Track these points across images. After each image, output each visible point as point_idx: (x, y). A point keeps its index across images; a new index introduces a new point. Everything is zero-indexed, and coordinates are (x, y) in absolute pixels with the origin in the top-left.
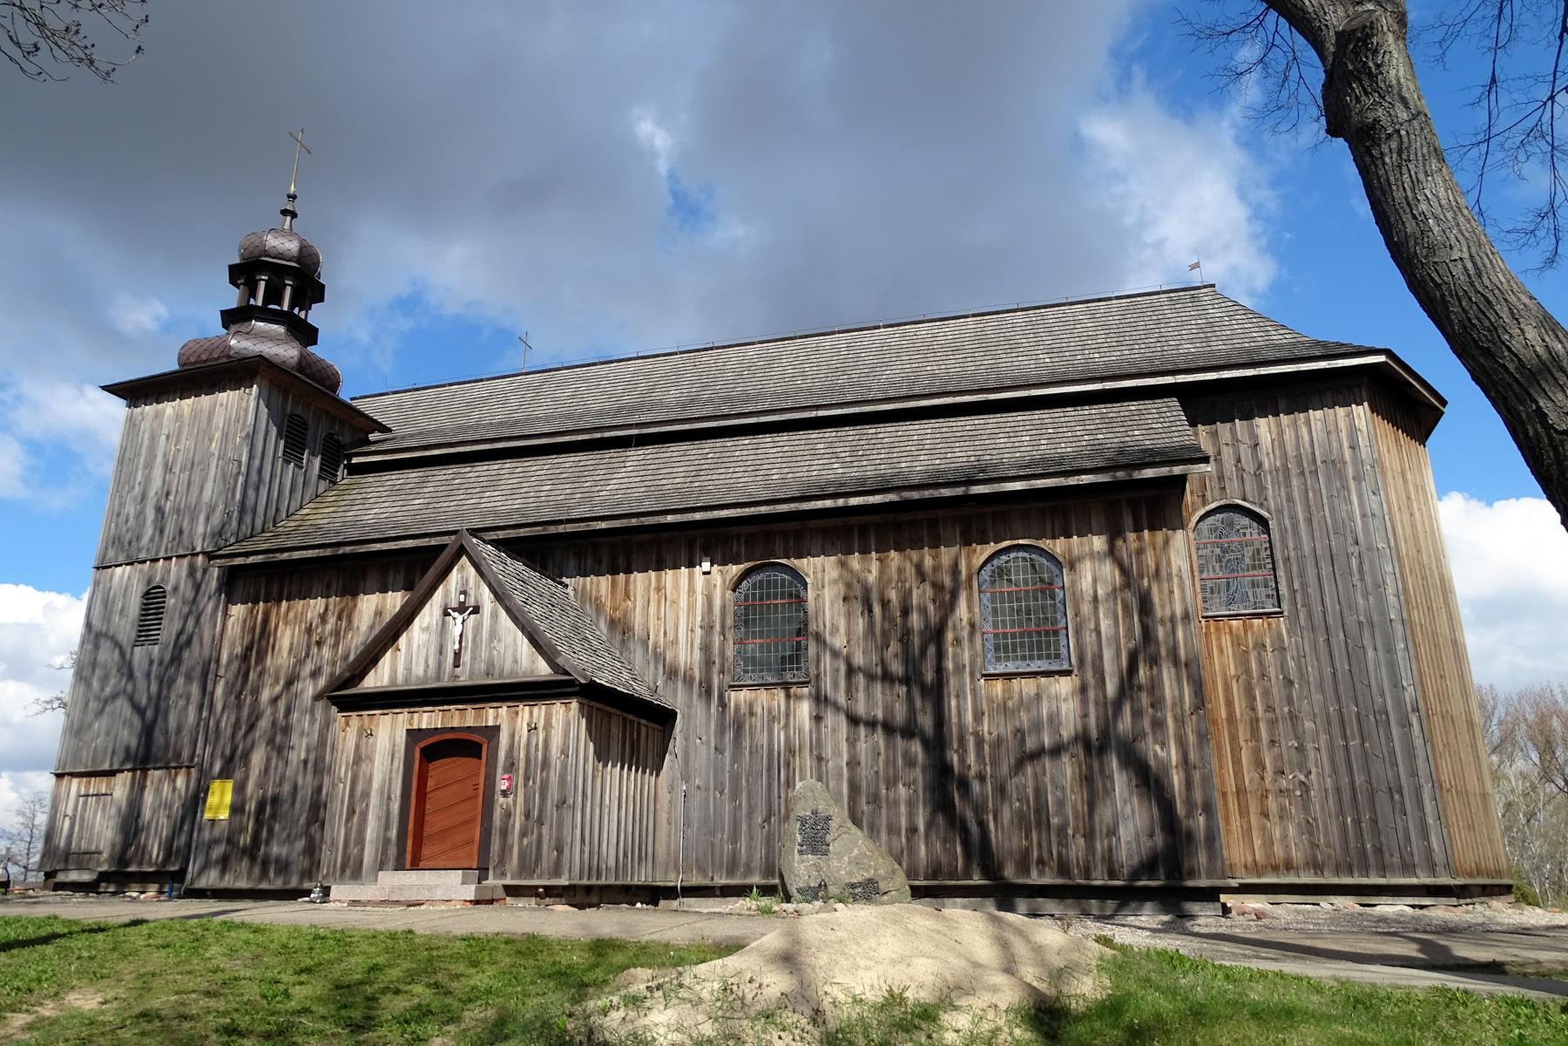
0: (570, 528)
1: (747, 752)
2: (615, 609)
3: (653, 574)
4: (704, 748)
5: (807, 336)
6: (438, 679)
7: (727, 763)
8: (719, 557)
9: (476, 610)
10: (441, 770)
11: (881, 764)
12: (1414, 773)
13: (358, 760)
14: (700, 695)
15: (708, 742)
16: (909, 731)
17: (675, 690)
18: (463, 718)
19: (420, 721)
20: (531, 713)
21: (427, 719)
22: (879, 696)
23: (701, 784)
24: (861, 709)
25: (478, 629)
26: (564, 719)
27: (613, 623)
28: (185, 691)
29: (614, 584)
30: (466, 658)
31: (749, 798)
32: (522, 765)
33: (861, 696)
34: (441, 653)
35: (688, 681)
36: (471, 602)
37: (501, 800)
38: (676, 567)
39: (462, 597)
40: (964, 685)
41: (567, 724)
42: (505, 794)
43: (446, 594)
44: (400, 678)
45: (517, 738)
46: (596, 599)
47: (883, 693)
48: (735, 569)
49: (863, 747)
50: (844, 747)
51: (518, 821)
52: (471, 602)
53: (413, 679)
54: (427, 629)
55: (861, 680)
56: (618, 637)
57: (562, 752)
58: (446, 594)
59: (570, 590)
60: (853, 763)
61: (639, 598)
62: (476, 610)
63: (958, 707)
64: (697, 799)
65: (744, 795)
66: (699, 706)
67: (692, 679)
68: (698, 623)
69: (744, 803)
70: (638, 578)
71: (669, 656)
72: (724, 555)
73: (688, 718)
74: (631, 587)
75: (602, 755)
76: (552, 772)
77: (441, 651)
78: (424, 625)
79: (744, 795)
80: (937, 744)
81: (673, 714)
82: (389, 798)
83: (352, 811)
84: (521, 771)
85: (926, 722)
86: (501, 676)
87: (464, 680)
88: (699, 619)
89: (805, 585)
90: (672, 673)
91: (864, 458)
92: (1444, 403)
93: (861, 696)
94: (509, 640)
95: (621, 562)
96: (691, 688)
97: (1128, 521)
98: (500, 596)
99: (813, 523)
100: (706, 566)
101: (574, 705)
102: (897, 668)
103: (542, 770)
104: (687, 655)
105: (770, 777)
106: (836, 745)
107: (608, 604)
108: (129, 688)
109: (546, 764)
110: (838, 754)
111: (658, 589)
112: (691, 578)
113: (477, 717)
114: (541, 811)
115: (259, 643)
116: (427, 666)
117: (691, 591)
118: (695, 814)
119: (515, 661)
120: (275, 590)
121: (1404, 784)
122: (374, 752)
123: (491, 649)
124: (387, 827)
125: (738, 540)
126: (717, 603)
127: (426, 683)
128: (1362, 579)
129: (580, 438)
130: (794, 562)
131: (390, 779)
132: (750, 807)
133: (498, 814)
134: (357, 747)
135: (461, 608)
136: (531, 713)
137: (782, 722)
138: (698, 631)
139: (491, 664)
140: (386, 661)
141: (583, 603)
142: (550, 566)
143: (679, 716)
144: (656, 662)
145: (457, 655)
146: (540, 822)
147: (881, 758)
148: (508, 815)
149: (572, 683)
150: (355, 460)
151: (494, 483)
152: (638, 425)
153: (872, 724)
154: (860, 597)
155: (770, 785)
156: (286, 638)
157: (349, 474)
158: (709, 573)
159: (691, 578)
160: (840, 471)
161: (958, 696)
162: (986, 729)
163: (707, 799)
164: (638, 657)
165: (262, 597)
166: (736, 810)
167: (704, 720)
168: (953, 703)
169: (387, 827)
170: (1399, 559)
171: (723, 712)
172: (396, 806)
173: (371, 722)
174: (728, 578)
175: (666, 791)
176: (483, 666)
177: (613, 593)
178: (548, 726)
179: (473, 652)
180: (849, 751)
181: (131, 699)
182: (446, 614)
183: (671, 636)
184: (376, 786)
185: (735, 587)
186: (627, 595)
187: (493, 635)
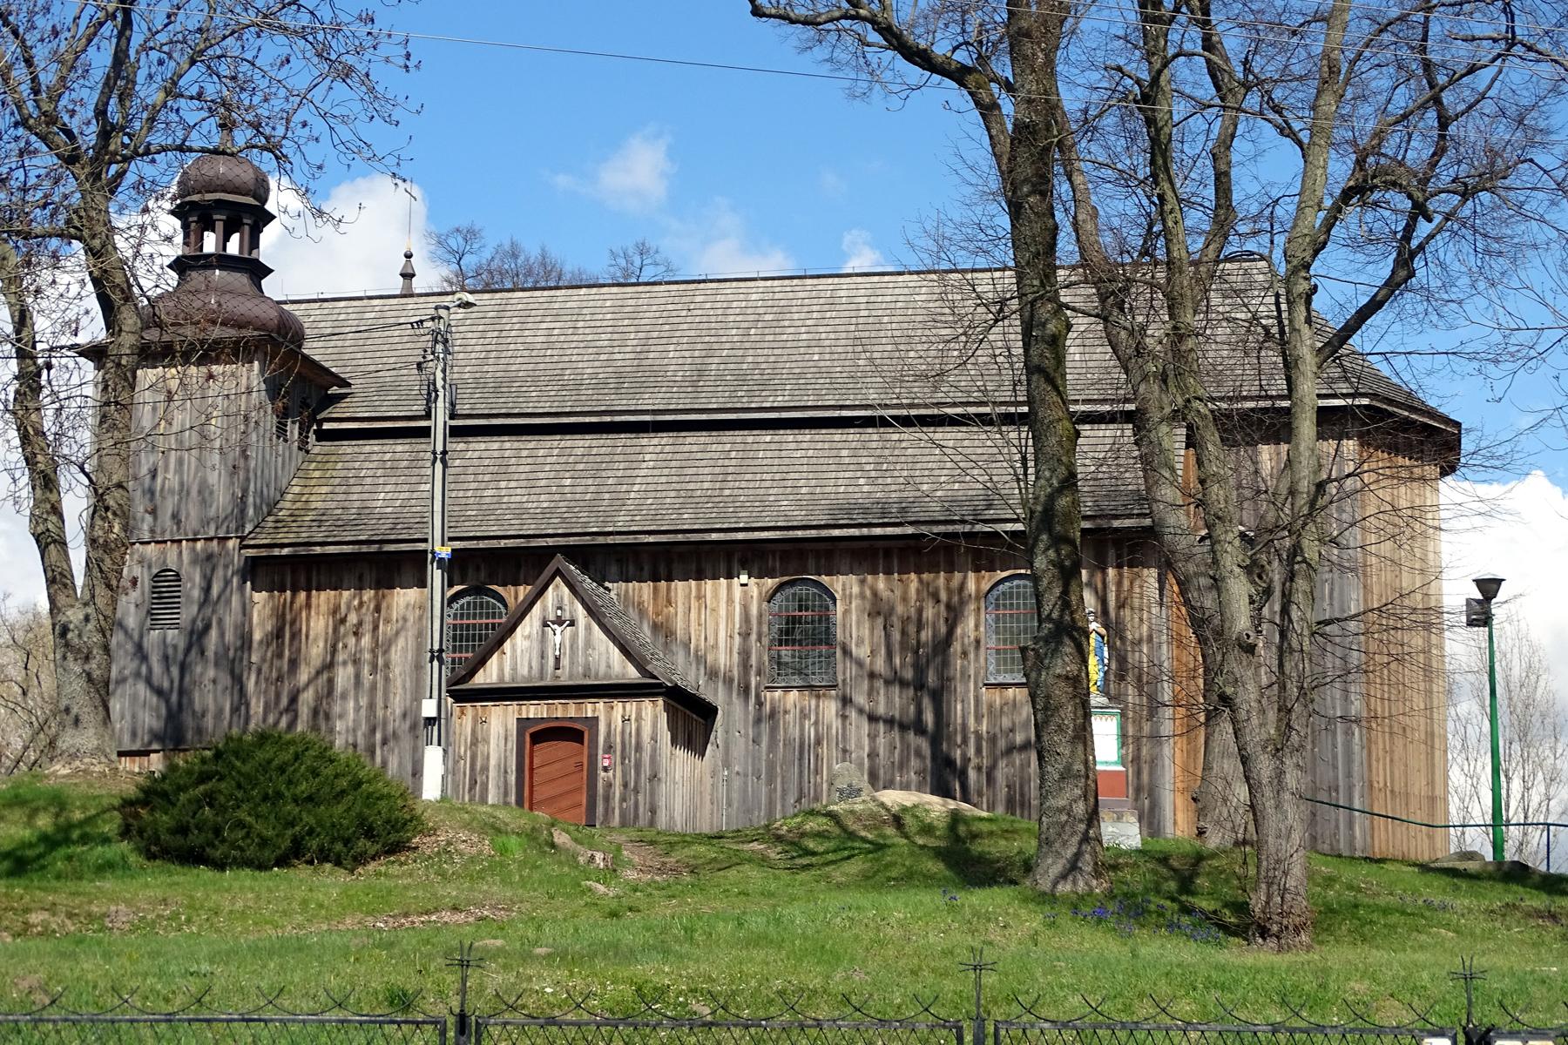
0: (619, 539)
1: (781, 744)
2: (658, 615)
3: (693, 583)
4: (743, 740)
5: (818, 277)
6: (542, 679)
7: (764, 754)
8: (756, 571)
9: (572, 624)
10: (546, 750)
11: (896, 755)
12: (1349, 775)
13: (475, 742)
14: (739, 694)
15: (747, 735)
16: (920, 729)
17: (716, 690)
18: (565, 710)
19: (528, 712)
20: (624, 708)
21: (535, 710)
22: (897, 699)
23: (741, 771)
24: (881, 710)
25: (574, 637)
26: (651, 715)
27: (656, 627)
28: (207, 674)
29: (656, 590)
30: (565, 662)
31: (783, 783)
32: (619, 747)
33: (882, 699)
34: (542, 658)
35: (728, 681)
36: (567, 616)
37: (603, 774)
38: (715, 577)
39: (559, 612)
40: (969, 691)
41: (655, 717)
42: (606, 769)
43: (544, 609)
44: (507, 677)
45: (613, 727)
46: (639, 604)
47: (900, 697)
48: (770, 583)
49: (881, 741)
50: (866, 741)
51: (617, 791)
52: (567, 616)
53: (519, 678)
54: (529, 637)
55: (880, 684)
56: (661, 639)
57: (652, 739)
58: (544, 609)
59: (613, 594)
60: (873, 755)
61: (680, 604)
62: (572, 624)
63: (963, 710)
64: (737, 783)
65: (779, 780)
66: (737, 702)
67: (731, 680)
68: (737, 631)
69: (779, 787)
70: (680, 587)
71: (710, 658)
72: (760, 569)
73: (728, 714)
74: (673, 594)
75: (674, 742)
76: (644, 754)
77: (543, 656)
78: (526, 633)
79: (779, 780)
80: (937, 738)
81: (715, 710)
82: (506, 772)
83: (473, 782)
84: (618, 753)
85: (929, 718)
86: (596, 677)
87: (565, 680)
88: (737, 626)
89: (834, 600)
90: (713, 674)
91: (888, 474)
92: (1458, 425)
93: (882, 699)
94: (603, 649)
95: (662, 570)
96: (730, 688)
97: (1111, 554)
98: (592, 612)
99: (843, 544)
100: (744, 578)
101: (660, 701)
102: (909, 674)
103: (636, 751)
104: (725, 658)
105: (800, 765)
106: (859, 740)
107: (651, 609)
108: (144, 669)
109: (639, 747)
110: (860, 746)
111: (699, 598)
112: (729, 588)
113: (578, 710)
114: (636, 783)
115: (285, 631)
116: (531, 667)
117: (730, 600)
118: (735, 796)
119: (609, 666)
120: (303, 579)
121: (1341, 783)
122: (489, 736)
123: (587, 656)
124: (506, 794)
125: (774, 557)
126: (754, 610)
127: (531, 681)
128: (1331, 604)
129: (587, 420)
130: (825, 579)
131: (506, 758)
132: (783, 790)
133: (600, 784)
134: (474, 732)
135: (560, 622)
136: (624, 708)
137: (813, 718)
138: (737, 639)
139: (587, 668)
140: (494, 661)
141: (626, 607)
142: (592, 568)
143: (720, 712)
144: (698, 663)
145: (557, 659)
146: (636, 791)
147: (897, 752)
148: (609, 785)
149: (660, 685)
150: (326, 426)
151: (502, 470)
152: (654, 412)
153: (890, 722)
154: (878, 610)
155: (801, 772)
156: (317, 625)
157: (318, 440)
158: (746, 585)
159: (729, 588)
160: (866, 488)
161: (963, 701)
162: (985, 728)
163: (745, 783)
164: (680, 658)
165: (289, 585)
166: (772, 792)
167: (742, 716)
168: (959, 707)
169: (506, 794)
170: (1365, 587)
171: (760, 710)
172: (512, 778)
173: (485, 713)
174: (764, 590)
175: (709, 776)
176: (580, 669)
177: (655, 599)
178: (639, 718)
179: (571, 658)
180: (870, 747)
181: (149, 681)
182: (545, 625)
183: (711, 641)
184: (493, 762)
185: (770, 599)
186: (669, 602)
187: (588, 644)
